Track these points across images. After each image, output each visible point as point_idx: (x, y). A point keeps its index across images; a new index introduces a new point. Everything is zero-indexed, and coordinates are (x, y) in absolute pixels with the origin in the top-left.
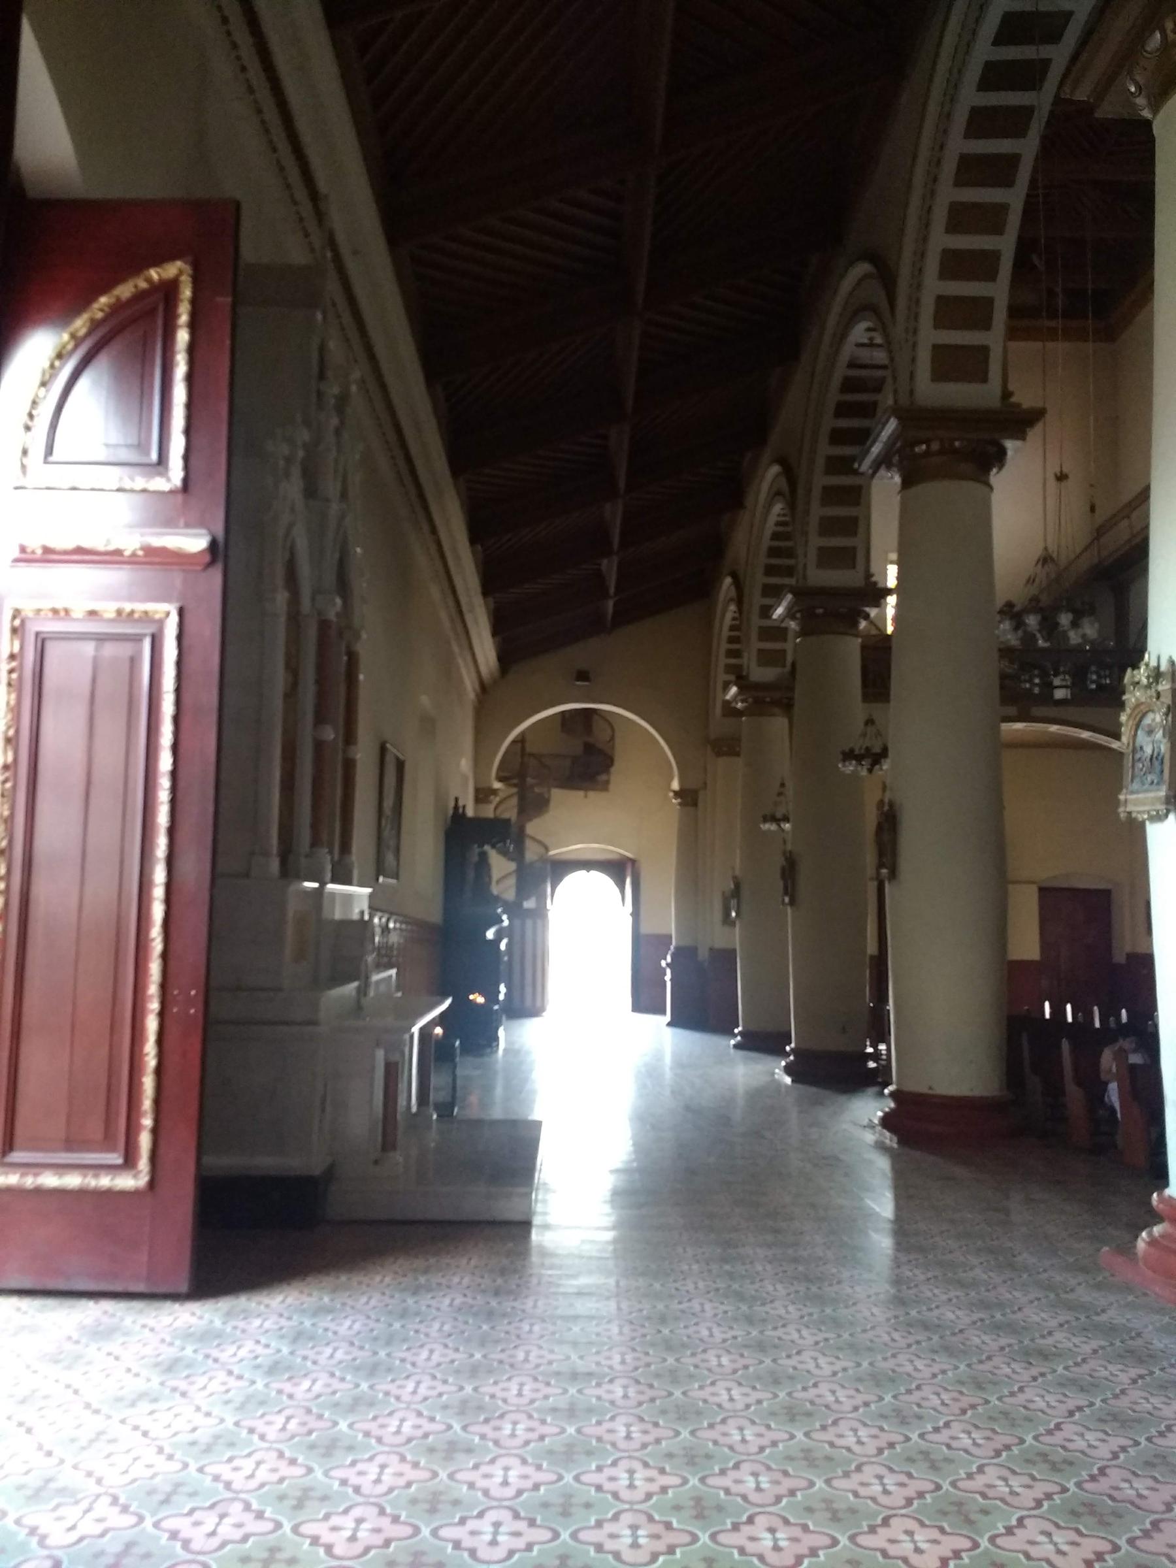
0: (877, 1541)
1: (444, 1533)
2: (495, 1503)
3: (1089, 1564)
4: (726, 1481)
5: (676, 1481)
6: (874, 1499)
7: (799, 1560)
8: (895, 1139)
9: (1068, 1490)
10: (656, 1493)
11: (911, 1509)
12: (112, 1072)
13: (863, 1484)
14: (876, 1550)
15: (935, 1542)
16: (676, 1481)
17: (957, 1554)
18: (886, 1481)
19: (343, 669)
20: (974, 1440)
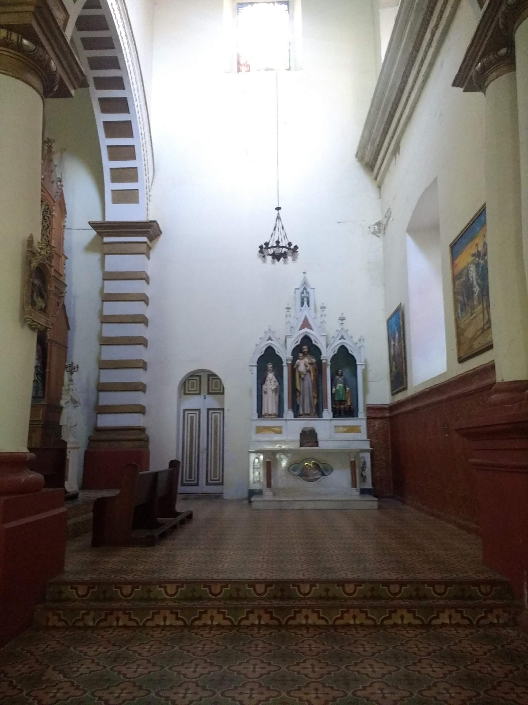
0: (433, 693)
1: (210, 693)
2: (256, 680)
3: (396, 702)
4: (269, 668)
5: (275, 668)
6: (428, 674)
7: (327, 702)
8: (286, 466)
9: (340, 669)
10: (387, 674)
11: (384, 679)
12: (178, 435)
13: (422, 668)
14: (431, 697)
15: (459, 693)
16: (275, 668)
17: (470, 698)
18: (374, 666)
19: (472, 48)
20: (471, 647)
